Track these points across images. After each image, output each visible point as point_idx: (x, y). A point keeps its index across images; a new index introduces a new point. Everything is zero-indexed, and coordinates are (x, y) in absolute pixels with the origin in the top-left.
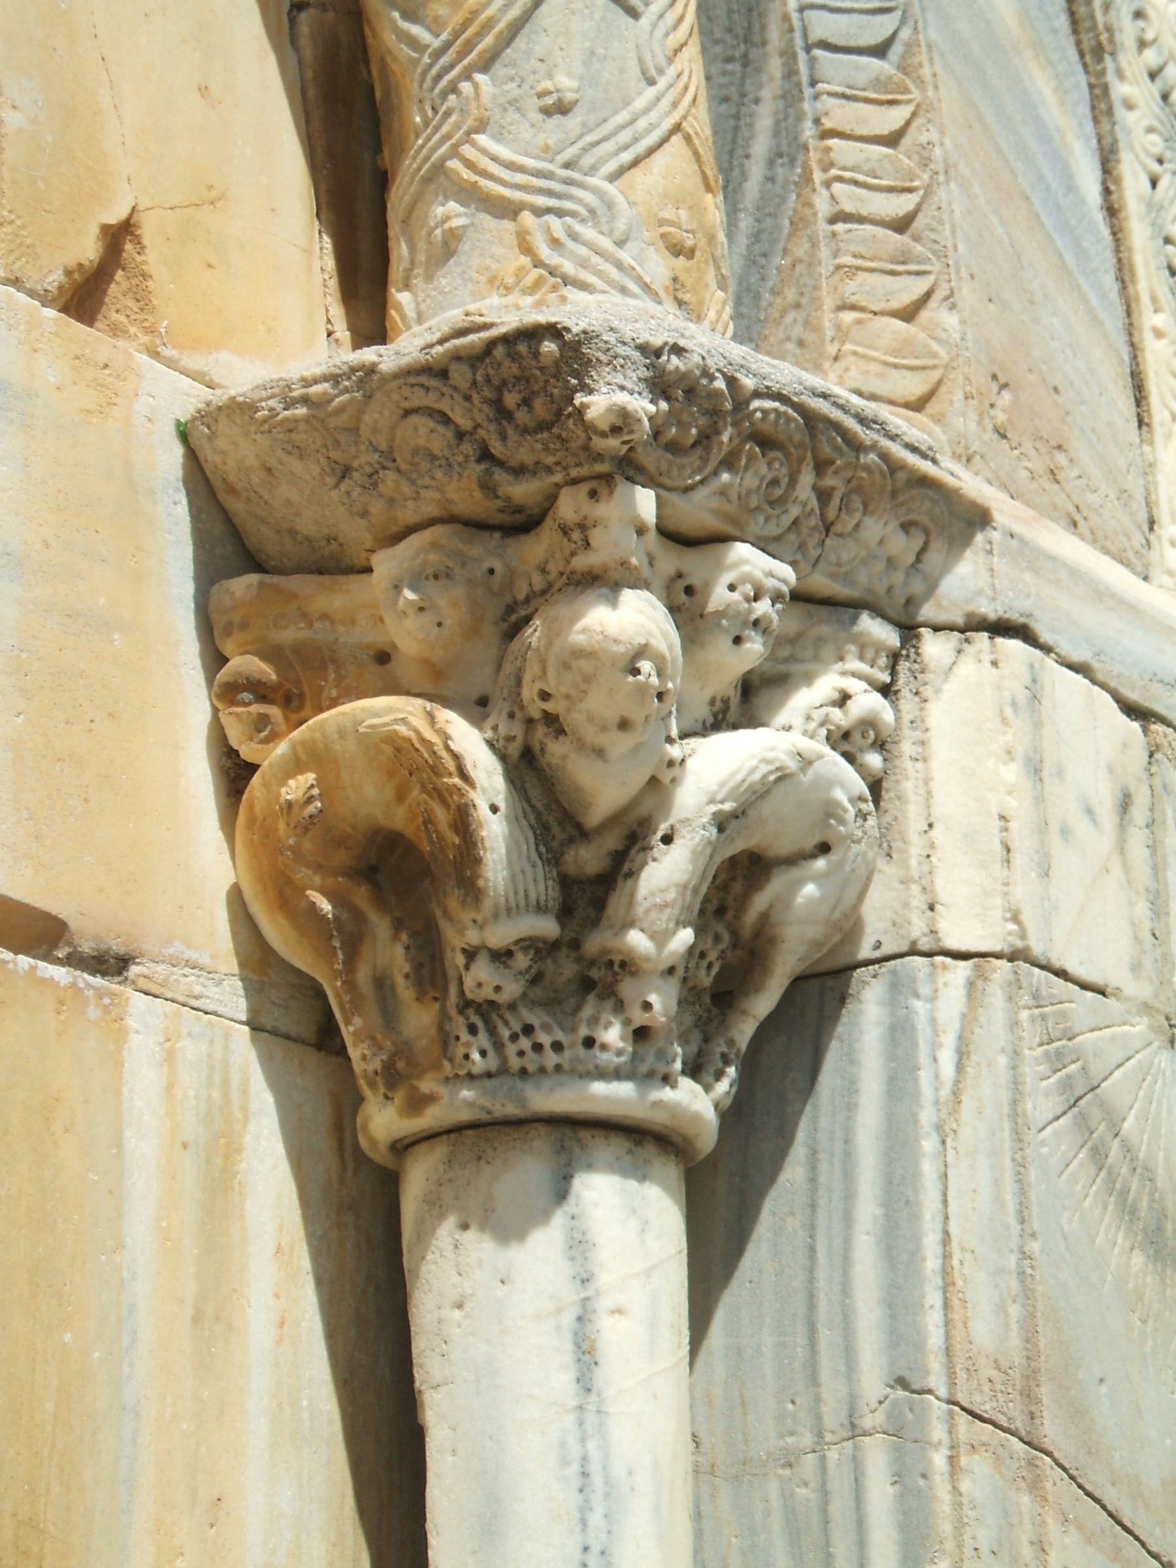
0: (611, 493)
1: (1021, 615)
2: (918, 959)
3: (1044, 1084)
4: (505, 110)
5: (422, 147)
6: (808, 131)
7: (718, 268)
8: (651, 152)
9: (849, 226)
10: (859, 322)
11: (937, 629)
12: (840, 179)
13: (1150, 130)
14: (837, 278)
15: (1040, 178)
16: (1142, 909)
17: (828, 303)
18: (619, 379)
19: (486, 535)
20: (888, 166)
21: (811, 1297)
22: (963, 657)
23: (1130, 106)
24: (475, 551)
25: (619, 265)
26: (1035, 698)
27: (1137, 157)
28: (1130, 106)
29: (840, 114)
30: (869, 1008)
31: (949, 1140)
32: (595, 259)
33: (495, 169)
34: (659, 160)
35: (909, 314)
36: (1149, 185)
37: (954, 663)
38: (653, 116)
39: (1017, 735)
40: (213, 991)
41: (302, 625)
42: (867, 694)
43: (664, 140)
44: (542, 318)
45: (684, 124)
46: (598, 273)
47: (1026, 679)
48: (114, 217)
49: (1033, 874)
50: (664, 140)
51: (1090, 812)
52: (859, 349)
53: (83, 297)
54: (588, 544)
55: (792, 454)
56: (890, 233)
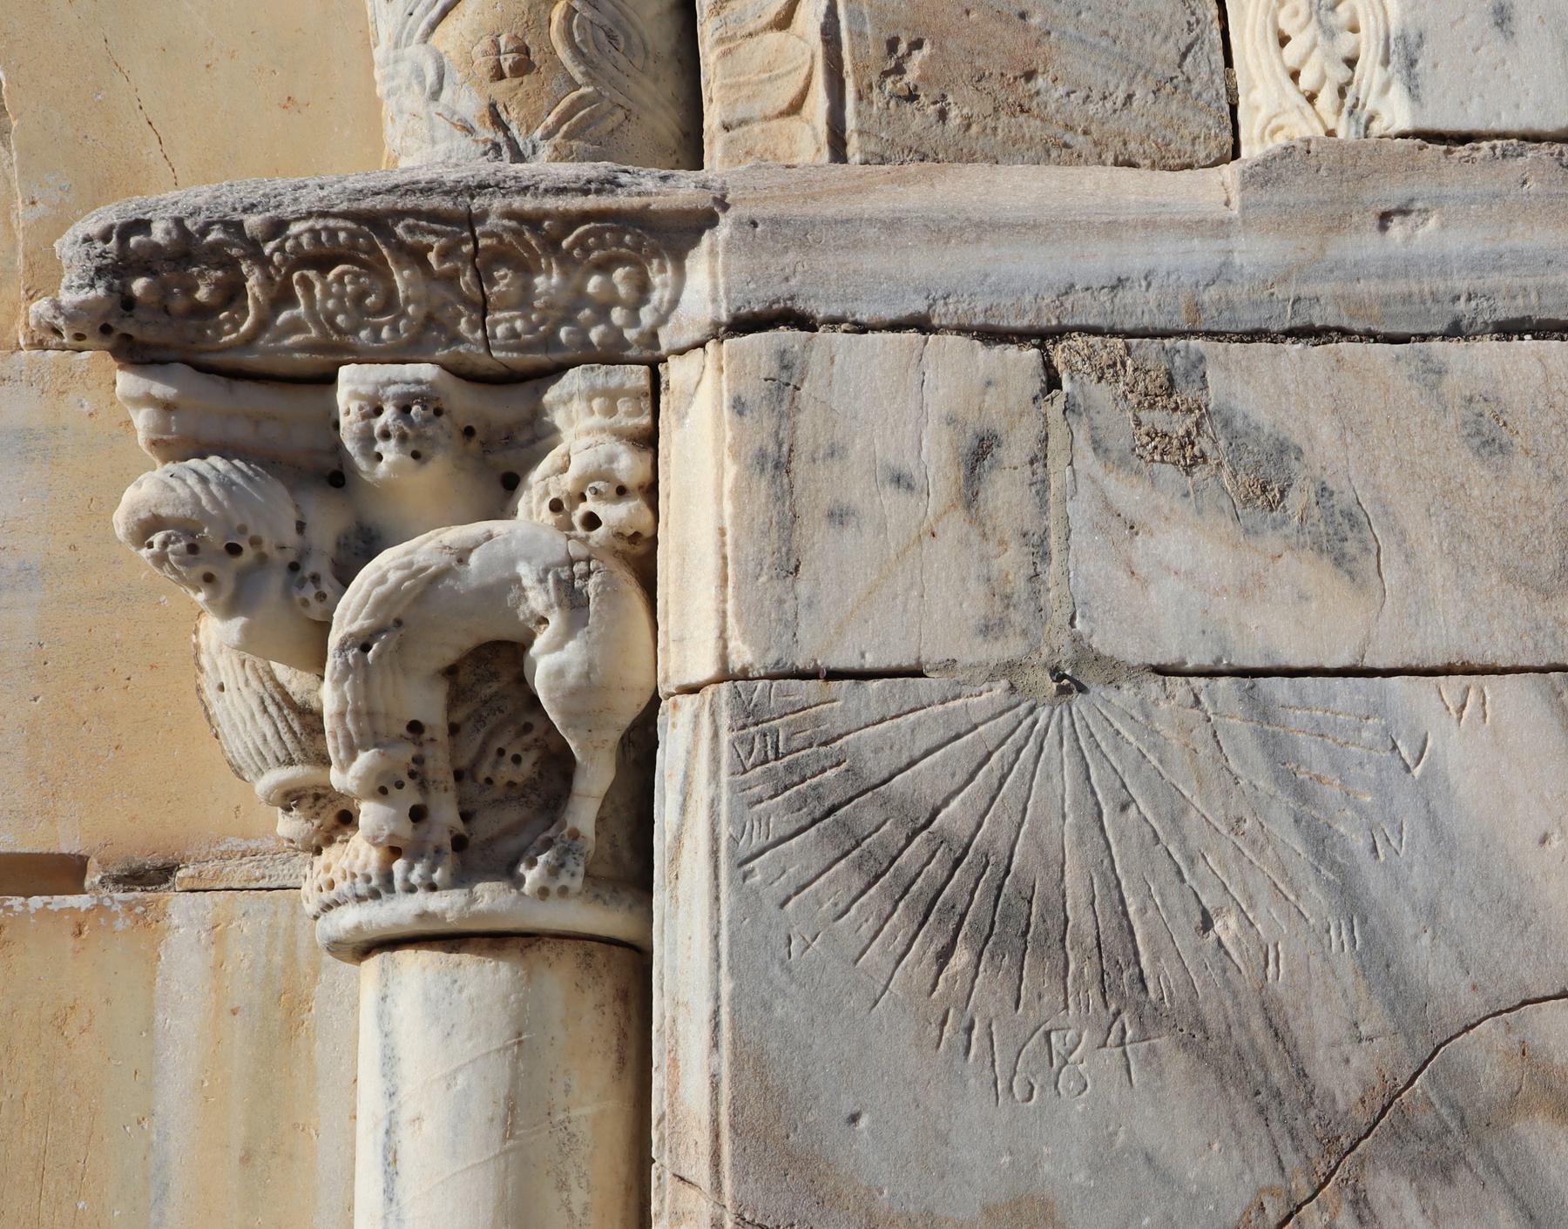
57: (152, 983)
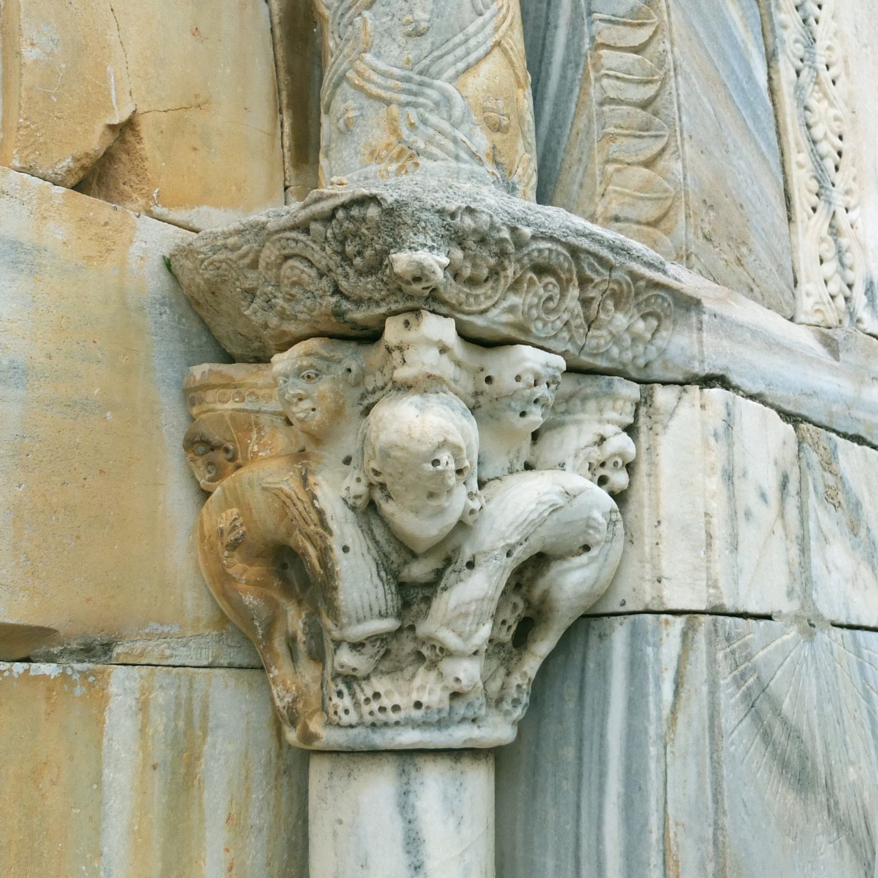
0: (418, 325)
1: (721, 370)
2: (650, 617)
3: (733, 701)
4: (382, 36)
5: (334, 63)
6: (586, 45)
7: (524, 138)
8: (478, 61)
9: (613, 107)
10: (618, 171)
11: (664, 383)
12: (608, 76)
13: (796, 41)
14: (604, 141)
15: (733, 72)
16: (794, 552)
17: (598, 159)
18: (421, 239)
19: (346, 345)
20: (638, 67)
21: (578, 839)
22: (682, 402)
23: (785, 27)
24: (338, 354)
25: (455, 141)
26: (729, 426)
27: (788, 57)
28: (785, 27)
29: (608, 34)
30: (619, 634)
31: (668, 746)
32: (439, 137)
33: (375, 77)
34: (485, 68)
35: (649, 164)
36: (795, 75)
37: (676, 406)
38: (481, 37)
39: (717, 455)
40: (183, 651)
41: (237, 399)
42: (618, 437)
43: (487, 54)
44: (366, 192)
45: (503, 42)
46: (440, 146)
47: (723, 414)
48: (117, 119)
49: (727, 552)
50: (487, 54)
51: (763, 496)
52: (618, 188)
53: (94, 178)
54: (405, 361)
55: (562, 279)
56: (639, 110)
57: (100, 743)
